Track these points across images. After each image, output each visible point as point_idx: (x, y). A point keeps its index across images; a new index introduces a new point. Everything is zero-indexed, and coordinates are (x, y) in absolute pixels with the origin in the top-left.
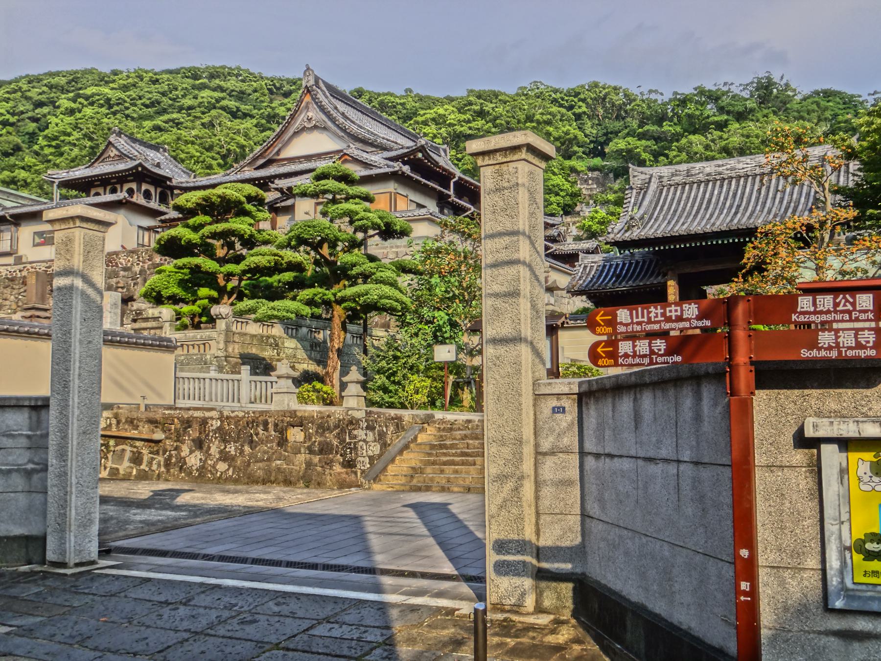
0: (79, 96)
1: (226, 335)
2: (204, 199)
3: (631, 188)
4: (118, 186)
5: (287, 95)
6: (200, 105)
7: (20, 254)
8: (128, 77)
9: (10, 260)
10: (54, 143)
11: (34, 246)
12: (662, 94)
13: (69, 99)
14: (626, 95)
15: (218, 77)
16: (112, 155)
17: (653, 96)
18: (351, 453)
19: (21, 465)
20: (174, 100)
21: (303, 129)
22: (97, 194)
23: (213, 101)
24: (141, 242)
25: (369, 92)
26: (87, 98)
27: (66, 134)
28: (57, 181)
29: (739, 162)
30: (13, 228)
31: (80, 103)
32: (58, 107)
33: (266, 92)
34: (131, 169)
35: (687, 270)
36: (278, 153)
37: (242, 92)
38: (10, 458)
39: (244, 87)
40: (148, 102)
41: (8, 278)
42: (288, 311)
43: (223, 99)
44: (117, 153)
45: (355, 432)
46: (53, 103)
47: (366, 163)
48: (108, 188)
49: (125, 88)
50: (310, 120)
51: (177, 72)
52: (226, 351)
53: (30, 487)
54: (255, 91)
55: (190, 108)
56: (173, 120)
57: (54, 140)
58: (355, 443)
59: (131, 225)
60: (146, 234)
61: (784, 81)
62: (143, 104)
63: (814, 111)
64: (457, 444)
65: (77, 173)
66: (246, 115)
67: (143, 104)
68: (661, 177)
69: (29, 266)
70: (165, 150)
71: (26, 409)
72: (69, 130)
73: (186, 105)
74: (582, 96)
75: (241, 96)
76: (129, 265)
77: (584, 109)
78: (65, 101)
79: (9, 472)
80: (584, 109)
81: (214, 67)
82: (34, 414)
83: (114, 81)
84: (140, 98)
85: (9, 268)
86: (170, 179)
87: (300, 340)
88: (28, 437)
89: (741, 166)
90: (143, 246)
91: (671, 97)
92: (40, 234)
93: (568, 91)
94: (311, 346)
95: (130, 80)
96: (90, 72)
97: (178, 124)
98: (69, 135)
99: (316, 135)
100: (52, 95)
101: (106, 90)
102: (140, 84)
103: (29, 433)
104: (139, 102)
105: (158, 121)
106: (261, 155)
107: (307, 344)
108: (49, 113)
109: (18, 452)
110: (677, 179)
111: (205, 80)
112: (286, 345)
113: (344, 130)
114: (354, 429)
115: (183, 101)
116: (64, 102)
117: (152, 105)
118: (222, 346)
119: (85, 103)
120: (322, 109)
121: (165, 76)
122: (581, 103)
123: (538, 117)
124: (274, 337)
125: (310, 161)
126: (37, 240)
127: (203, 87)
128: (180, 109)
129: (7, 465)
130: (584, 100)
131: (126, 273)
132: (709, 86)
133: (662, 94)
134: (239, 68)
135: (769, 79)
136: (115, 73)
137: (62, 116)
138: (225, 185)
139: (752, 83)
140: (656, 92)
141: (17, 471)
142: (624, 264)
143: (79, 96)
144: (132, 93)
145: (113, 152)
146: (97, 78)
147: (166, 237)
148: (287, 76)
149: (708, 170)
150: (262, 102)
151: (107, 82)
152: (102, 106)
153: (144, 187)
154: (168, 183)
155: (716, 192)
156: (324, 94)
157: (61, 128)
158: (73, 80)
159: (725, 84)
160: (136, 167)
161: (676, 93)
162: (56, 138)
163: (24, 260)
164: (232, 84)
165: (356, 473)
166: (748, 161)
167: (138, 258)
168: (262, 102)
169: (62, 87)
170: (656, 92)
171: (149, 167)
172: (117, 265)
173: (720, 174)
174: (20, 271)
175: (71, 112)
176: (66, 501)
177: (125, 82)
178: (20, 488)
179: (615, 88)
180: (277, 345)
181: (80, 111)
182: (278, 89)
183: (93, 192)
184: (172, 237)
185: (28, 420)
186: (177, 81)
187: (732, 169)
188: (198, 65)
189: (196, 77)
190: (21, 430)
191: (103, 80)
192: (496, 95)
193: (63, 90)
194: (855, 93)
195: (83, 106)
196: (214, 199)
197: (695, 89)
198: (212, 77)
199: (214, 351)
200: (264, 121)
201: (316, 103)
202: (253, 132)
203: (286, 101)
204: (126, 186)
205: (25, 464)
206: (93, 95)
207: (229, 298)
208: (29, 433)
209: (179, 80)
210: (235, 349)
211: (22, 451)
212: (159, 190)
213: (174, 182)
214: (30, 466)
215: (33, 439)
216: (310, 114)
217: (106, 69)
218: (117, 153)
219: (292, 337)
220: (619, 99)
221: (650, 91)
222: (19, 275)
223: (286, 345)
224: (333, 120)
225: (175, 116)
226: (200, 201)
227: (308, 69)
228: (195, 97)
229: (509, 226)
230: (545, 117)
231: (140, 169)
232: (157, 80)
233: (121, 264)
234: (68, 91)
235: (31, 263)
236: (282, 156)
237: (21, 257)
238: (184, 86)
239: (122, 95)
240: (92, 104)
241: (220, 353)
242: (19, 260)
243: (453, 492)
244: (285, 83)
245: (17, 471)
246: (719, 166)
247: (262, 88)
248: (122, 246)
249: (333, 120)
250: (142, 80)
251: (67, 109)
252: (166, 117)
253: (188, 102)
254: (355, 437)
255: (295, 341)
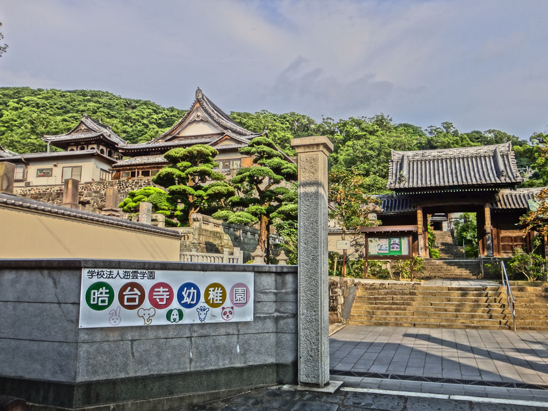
0: (20, 101)
1: (199, 231)
2: (188, 152)
3: (392, 161)
4: (85, 146)
5: (134, 108)
6: (88, 110)
7: (28, 180)
8: (48, 93)
9: (23, 184)
10: (6, 125)
11: (37, 177)
12: (333, 120)
13: (14, 102)
14: (308, 120)
15: (96, 96)
16: (83, 129)
17: (329, 121)
18: (333, 302)
19: (271, 314)
20: (74, 106)
21: (195, 121)
22: (72, 150)
23: (96, 108)
24: (101, 178)
25: (177, 110)
26: (25, 102)
27: (13, 120)
28: (50, 141)
29: (450, 151)
30: (24, 166)
31: (21, 105)
32: (8, 106)
33: (123, 106)
34: (96, 137)
35: (429, 205)
36: (178, 134)
37: (110, 105)
38: (265, 309)
39: (111, 102)
40: (59, 107)
41: (21, 195)
42: (247, 218)
43: (101, 107)
44: (86, 128)
45: (336, 290)
46: (6, 104)
47: (238, 141)
48: (79, 147)
49: (47, 98)
50: (198, 116)
51: (74, 92)
52: (199, 239)
53: (277, 328)
54: (117, 105)
55: (83, 111)
56: (74, 117)
57: (6, 123)
58: (336, 297)
59: (97, 167)
60: (104, 173)
61: (389, 118)
62: (56, 108)
63: (403, 133)
64: (386, 298)
65: (62, 137)
66: (113, 117)
67: (56, 108)
68: (408, 156)
69: (35, 188)
70: (110, 128)
71: (273, 274)
72: (15, 119)
73: (80, 110)
74: (287, 119)
75: (110, 107)
76: (98, 190)
77: (288, 125)
78: (12, 103)
79: (265, 318)
80: (288, 125)
81: (94, 91)
82: (279, 278)
83: (40, 94)
84: (55, 104)
85: (22, 189)
86: (117, 144)
87: (230, 235)
88: (275, 294)
89: (451, 153)
90: (103, 180)
91: (339, 121)
92: (40, 170)
93: (281, 116)
94: (235, 239)
95: (49, 94)
96: (27, 88)
97: (76, 119)
98: (16, 121)
99: (201, 125)
100: (5, 99)
101: (36, 99)
102: (54, 97)
103: (275, 291)
104: (55, 106)
105: (66, 117)
106: (169, 134)
107: (233, 237)
108: (3, 109)
109: (269, 304)
110: (417, 158)
111: (89, 97)
112: (225, 238)
113: (219, 123)
114: (335, 288)
115: (79, 107)
116: (12, 103)
117: (62, 108)
118: (197, 237)
119: (24, 105)
120: (206, 111)
121: (69, 94)
122: (287, 122)
123: (270, 127)
124: (219, 233)
125: (197, 138)
126: (39, 174)
127: (89, 101)
128: (77, 111)
129: (263, 313)
130: (288, 121)
131: (96, 194)
132: (356, 118)
133: (333, 120)
134: (107, 92)
135: (382, 116)
136: (40, 90)
137: (10, 111)
138: (198, 145)
139: (374, 118)
140: (330, 119)
141: (269, 318)
142: (388, 201)
143: (20, 101)
144: (51, 101)
145: (83, 127)
146: (30, 92)
147: (164, 173)
148: (133, 98)
149: (433, 154)
150: (121, 110)
151: (36, 95)
152: (34, 107)
153: (101, 147)
154: (116, 146)
155: (483, 163)
156: (207, 103)
157: (11, 117)
158: (17, 92)
159: (363, 117)
160: (99, 136)
161: (341, 120)
162: (7, 122)
163: (31, 185)
164: (103, 100)
165: (337, 314)
166: (455, 151)
167: (104, 186)
168: (121, 110)
169: (11, 96)
170: (330, 119)
171: (106, 137)
172: (90, 189)
173: (440, 156)
174: (29, 191)
175: (16, 109)
176: (318, 340)
177: (46, 95)
178: (271, 330)
179: (303, 116)
180: (221, 238)
181: (21, 109)
182: (128, 104)
183: (69, 149)
184: (169, 173)
185: (274, 282)
186: (75, 96)
187: (446, 154)
188: (85, 89)
189: (84, 95)
190: (271, 289)
191: (34, 93)
192: (248, 115)
193: (11, 97)
194: (418, 126)
195: (23, 106)
196: (195, 152)
197: (350, 119)
198: (93, 96)
199: (191, 239)
200: (123, 120)
201: (203, 108)
202: (119, 126)
203: (135, 110)
204: (90, 147)
205: (273, 313)
206: (28, 101)
207: (195, 210)
208: (275, 291)
209: (76, 96)
210: (203, 239)
211: (271, 304)
212: (108, 149)
213: (119, 146)
214: (276, 314)
215: (279, 295)
216: (199, 114)
217: (35, 87)
218: (86, 128)
219: (226, 233)
220: (305, 121)
221: (328, 118)
222: (28, 193)
223: (225, 238)
224: (212, 118)
225: (75, 114)
226: (185, 153)
227: (199, 89)
228: (85, 106)
229: (313, 179)
230: (274, 128)
231: (101, 137)
232: (64, 95)
233: (93, 189)
234: (14, 98)
235: (36, 186)
236: (181, 135)
237: (29, 183)
238: (79, 99)
239: (46, 102)
240: (28, 105)
241: (195, 241)
242: (28, 185)
243: (404, 326)
244: (132, 102)
245: (269, 318)
246: (439, 152)
247: (121, 103)
248: (93, 179)
249: (212, 118)
250: (55, 95)
251: (13, 107)
252: (70, 115)
253: (81, 108)
254: (336, 293)
255: (228, 235)
